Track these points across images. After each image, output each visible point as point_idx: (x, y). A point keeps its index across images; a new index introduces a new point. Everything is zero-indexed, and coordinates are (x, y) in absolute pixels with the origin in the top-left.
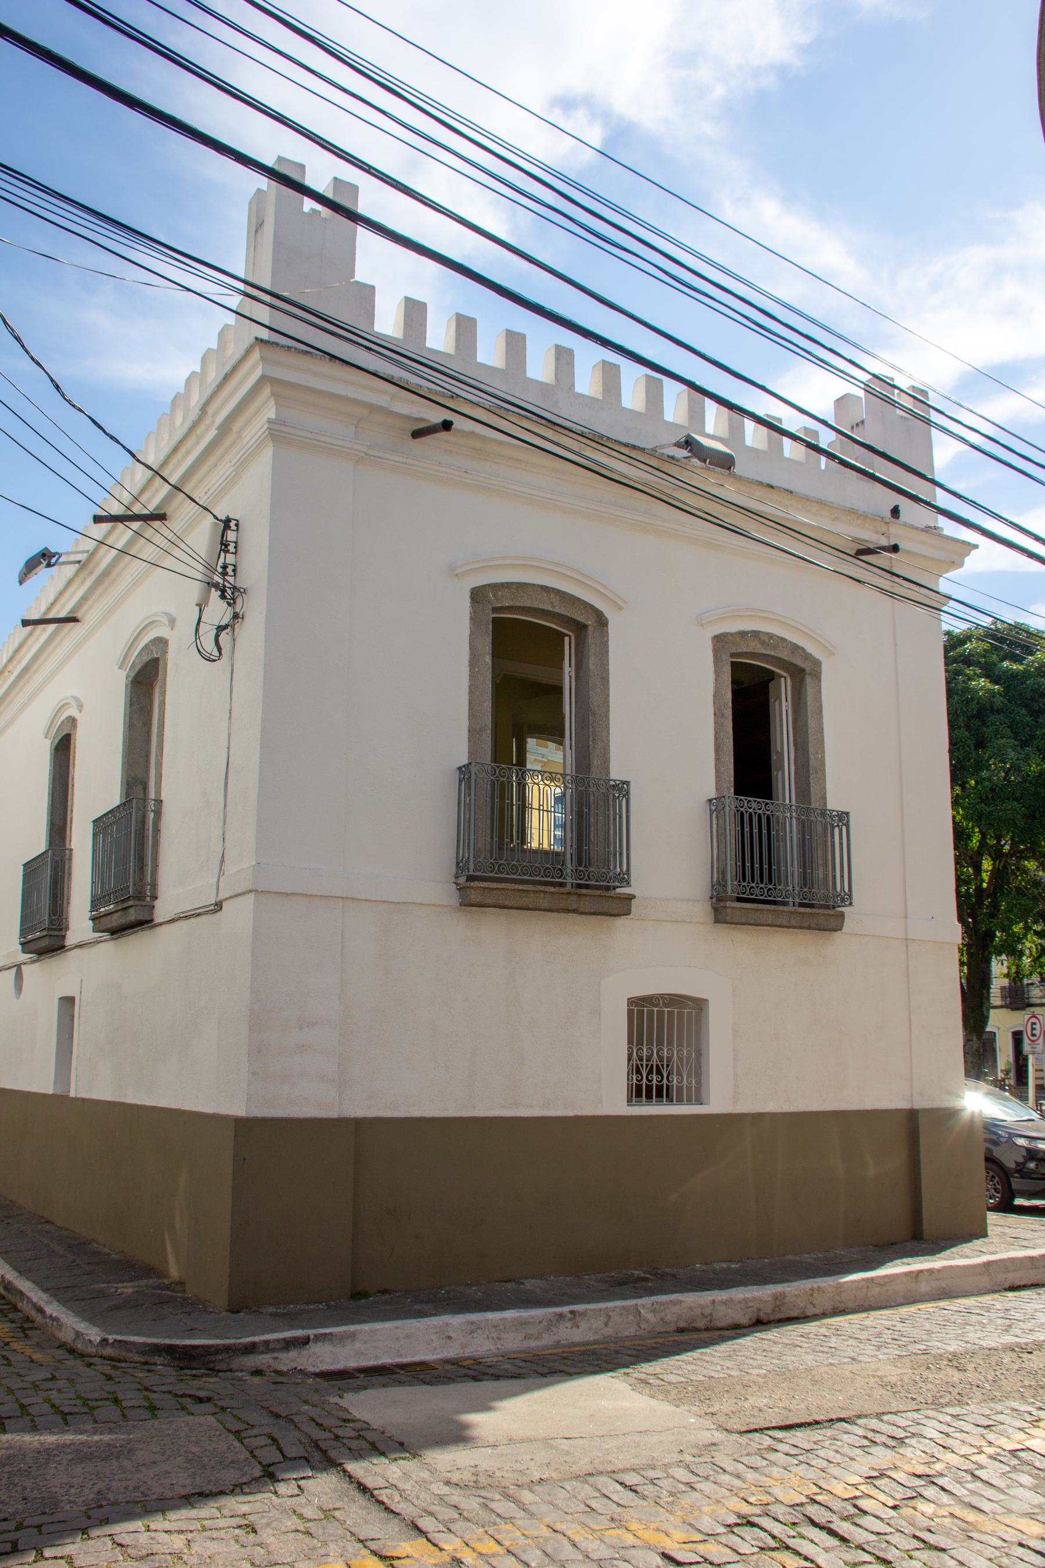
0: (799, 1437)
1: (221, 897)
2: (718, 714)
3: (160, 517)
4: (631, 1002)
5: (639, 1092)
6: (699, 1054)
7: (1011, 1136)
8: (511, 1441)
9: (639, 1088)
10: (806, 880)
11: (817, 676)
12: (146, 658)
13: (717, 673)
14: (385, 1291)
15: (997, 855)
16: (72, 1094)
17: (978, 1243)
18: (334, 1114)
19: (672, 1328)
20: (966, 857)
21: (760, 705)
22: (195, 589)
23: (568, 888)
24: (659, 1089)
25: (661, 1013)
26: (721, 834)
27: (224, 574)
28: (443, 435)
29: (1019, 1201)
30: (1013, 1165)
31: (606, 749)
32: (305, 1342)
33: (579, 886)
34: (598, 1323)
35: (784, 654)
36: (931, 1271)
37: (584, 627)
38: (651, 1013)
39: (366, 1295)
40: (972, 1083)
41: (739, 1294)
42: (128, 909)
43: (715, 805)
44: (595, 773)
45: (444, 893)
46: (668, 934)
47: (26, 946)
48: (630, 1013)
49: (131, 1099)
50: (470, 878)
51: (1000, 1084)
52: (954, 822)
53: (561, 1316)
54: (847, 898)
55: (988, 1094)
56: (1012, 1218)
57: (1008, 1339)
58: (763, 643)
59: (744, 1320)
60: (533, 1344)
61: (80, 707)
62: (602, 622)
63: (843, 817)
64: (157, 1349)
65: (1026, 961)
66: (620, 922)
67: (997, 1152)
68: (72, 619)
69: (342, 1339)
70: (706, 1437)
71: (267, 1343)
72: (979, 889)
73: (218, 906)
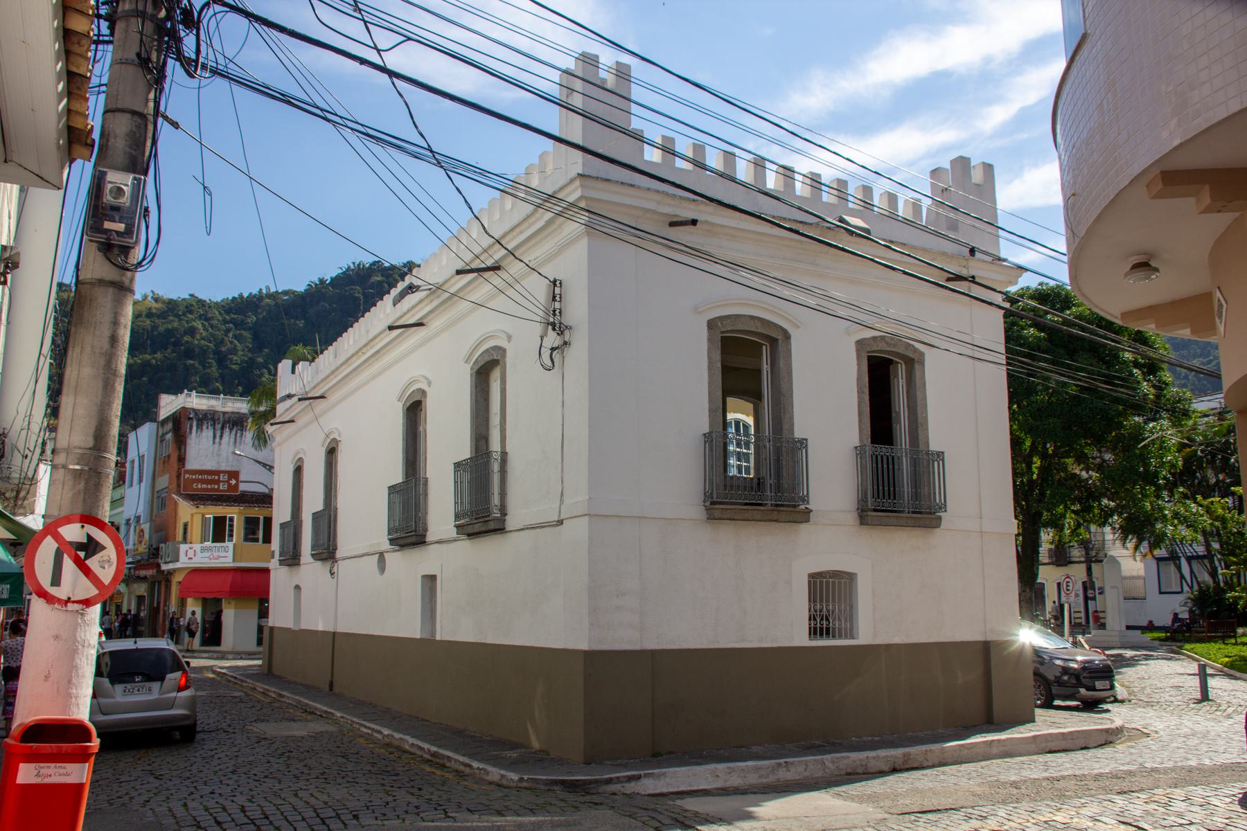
0: (930, 816)
1: (562, 517)
2: (860, 392)
3: (496, 268)
4: (812, 576)
5: (814, 632)
6: (851, 607)
7: (1052, 658)
8: (777, 818)
9: (815, 629)
10: (916, 496)
11: (922, 363)
12: (487, 358)
13: (859, 365)
14: (671, 753)
15: (1044, 456)
16: (438, 638)
17: (1029, 726)
18: (638, 648)
19: (843, 772)
20: (1019, 456)
21: (886, 379)
22: (538, 329)
23: (769, 507)
24: (828, 629)
25: (827, 583)
26: (863, 468)
27: (554, 315)
28: (690, 228)
29: (1057, 702)
30: (1053, 678)
31: (792, 418)
32: (638, 778)
33: (777, 505)
34: (801, 768)
35: (901, 350)
36: (999, 741)
37: (777, 340)
38: (821, 582)
39: (662, 754)
40: (1026, 623)
41: (882, 753)
42: (482, 518)
43: (860, 451)
44: (785, 434)
45: (695, 510)
46: (831, 534)
47: (392, 541)
48: (809, 582)
49: (490, 640)
50: (713, 503)
51: (1046, 624)
52: (1011, 433)
53: (780, 764)
54: (943, 507)
55: (1038, 631)
56: (1052, 712)
57: (1046, 774)
58: (887, 343)
59: (886, 768)
60: (764, 780)
61: (429, 384)
62: (787, 336)
63: (940, 455)
64: (555, 782)
65: (1067, 532)
66: (803, 526)
67: (1042, 670)
68: (419, 324)
69: (659, 776)
70: (880, 816)
71: (618, 778)
72: (1031, 482)
73: (560, 522)
